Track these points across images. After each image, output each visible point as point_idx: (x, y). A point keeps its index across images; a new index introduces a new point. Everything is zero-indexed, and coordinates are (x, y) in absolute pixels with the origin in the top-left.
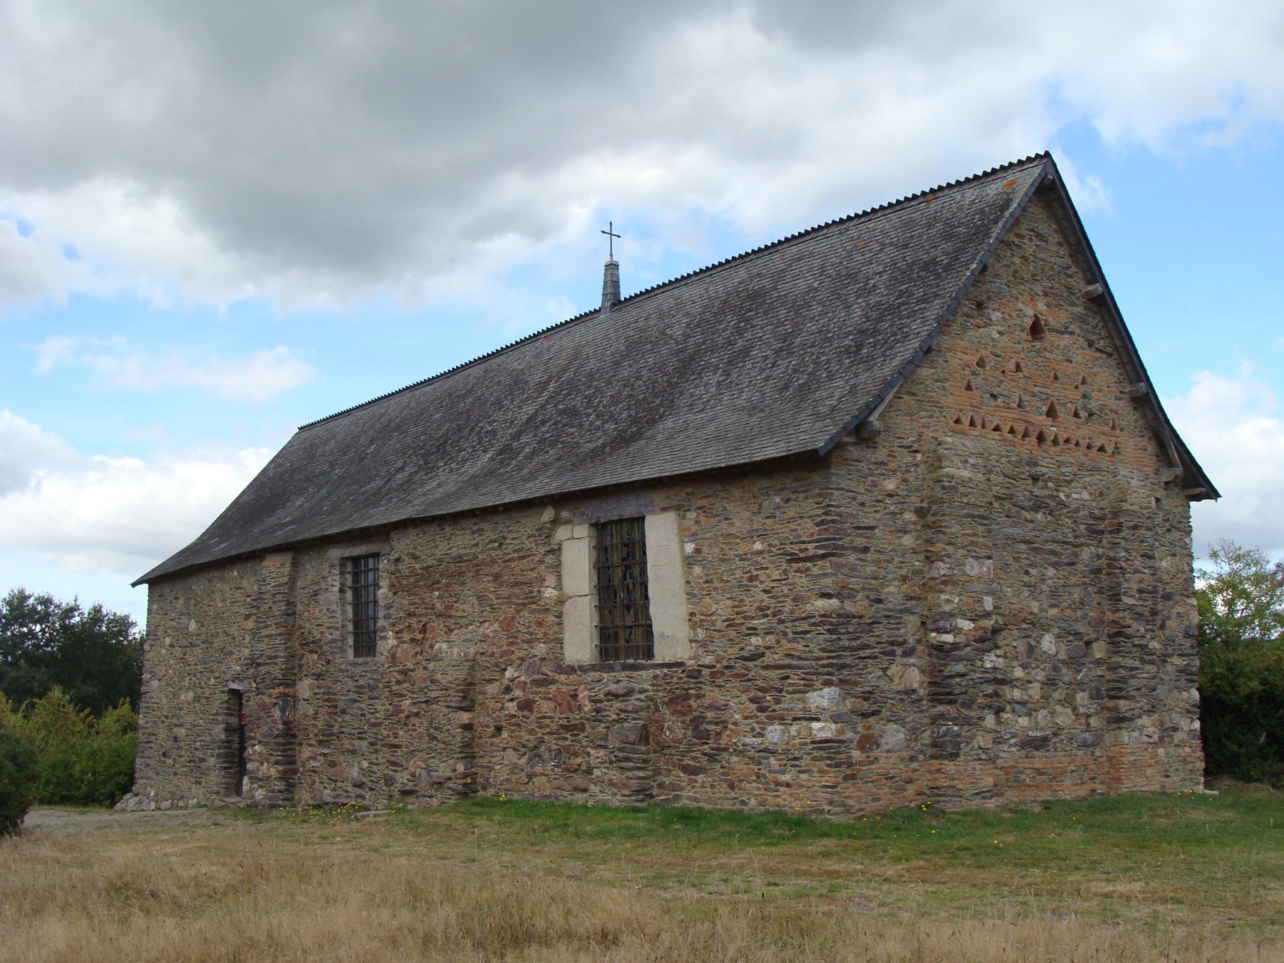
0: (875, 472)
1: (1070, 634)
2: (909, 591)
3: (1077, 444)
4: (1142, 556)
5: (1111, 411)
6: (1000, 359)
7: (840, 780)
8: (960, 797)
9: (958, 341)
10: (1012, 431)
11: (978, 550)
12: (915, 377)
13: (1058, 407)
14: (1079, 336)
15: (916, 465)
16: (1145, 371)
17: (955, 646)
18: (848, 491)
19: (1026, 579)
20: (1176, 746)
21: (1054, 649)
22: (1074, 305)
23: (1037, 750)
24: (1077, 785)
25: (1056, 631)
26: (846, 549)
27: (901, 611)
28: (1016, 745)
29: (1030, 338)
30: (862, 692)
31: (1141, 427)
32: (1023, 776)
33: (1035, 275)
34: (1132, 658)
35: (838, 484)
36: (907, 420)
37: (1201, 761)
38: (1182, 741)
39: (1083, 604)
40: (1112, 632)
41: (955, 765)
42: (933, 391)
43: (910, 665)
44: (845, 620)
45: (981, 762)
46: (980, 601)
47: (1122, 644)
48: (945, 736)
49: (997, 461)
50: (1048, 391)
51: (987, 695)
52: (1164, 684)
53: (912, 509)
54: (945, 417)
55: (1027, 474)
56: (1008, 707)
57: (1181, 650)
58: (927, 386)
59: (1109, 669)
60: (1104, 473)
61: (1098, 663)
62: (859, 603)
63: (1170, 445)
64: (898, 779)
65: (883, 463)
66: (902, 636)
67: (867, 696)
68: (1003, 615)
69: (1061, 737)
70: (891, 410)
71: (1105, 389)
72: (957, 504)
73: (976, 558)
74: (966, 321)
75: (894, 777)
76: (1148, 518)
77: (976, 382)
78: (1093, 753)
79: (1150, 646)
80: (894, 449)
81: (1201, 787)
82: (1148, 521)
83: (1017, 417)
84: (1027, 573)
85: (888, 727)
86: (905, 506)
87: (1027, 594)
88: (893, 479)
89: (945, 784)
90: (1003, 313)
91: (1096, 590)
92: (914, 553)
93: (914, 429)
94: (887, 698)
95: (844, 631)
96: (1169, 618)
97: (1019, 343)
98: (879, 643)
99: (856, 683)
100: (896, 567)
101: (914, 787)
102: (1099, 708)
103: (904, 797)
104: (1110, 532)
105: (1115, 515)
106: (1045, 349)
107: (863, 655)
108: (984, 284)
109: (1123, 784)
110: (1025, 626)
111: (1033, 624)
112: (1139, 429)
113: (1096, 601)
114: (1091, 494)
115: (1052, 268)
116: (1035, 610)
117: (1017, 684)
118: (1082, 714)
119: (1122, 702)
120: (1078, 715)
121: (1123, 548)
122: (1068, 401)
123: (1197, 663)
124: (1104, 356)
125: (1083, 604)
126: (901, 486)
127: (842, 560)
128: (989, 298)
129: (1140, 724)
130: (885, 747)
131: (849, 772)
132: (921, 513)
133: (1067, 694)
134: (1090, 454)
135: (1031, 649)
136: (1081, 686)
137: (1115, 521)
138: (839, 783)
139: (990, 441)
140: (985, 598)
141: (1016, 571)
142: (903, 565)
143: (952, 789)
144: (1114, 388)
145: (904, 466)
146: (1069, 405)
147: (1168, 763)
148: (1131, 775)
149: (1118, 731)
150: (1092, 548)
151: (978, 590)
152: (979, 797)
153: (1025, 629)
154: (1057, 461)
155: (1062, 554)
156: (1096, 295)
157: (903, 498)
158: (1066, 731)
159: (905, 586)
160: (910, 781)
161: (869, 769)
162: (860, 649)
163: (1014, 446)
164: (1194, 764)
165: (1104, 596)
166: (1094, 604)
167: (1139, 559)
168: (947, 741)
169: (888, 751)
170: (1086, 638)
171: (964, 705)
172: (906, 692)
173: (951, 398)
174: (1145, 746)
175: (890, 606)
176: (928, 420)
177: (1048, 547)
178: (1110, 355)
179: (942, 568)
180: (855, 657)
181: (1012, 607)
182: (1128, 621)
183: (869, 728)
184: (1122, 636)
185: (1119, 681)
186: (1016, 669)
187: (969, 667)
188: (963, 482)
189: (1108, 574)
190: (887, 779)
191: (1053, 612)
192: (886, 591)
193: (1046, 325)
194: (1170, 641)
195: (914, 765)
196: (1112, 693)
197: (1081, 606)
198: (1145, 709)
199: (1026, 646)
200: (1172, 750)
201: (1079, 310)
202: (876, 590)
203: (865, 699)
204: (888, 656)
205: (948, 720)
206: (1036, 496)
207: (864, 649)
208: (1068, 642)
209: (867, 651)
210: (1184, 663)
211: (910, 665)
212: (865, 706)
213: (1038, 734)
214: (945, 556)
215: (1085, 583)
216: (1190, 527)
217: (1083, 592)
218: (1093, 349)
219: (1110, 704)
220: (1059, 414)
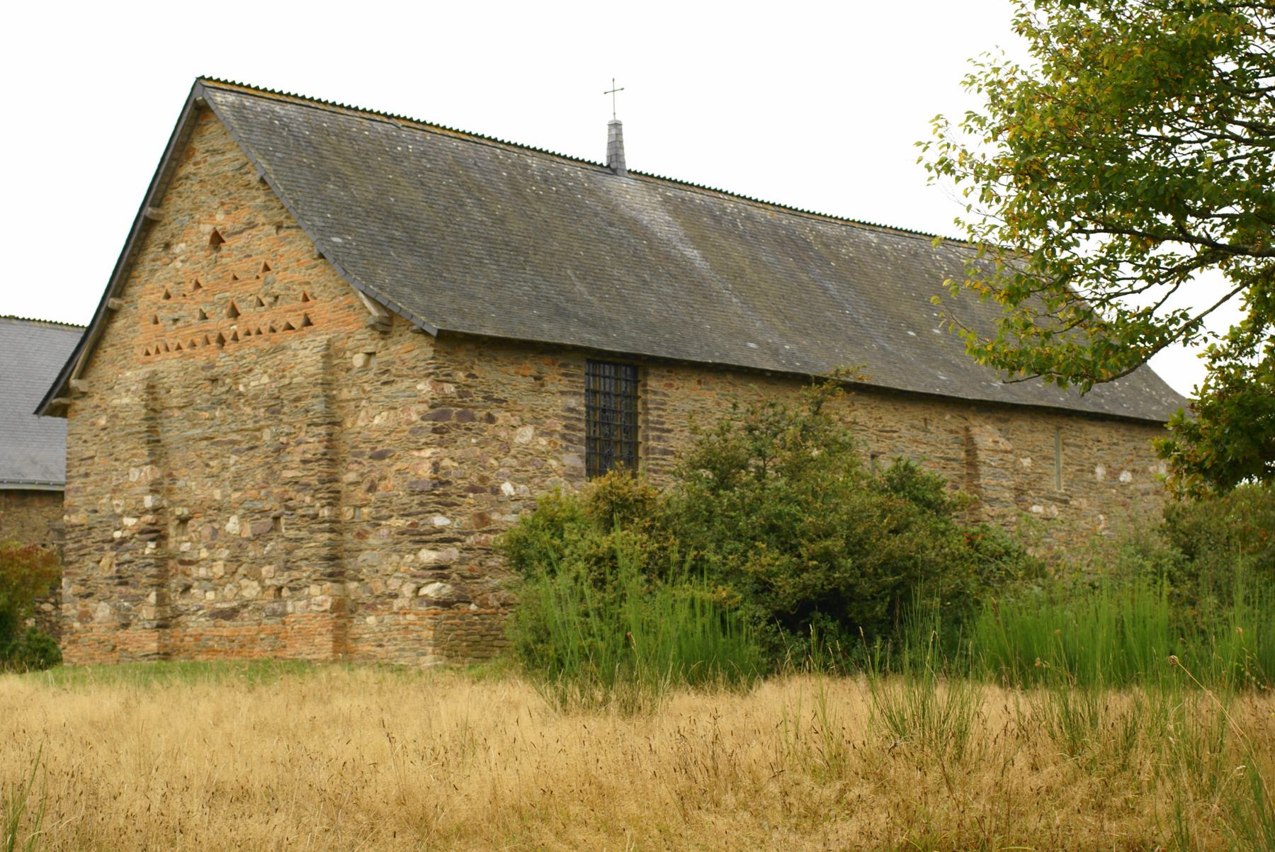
3: (259, 332)
19: (208, 470)
22: (254, 198)
25: (241, 512)
32: (210, 643)
46: (141, 501)
52: (373, 550)
56: (196, 584)
57: (405, 509)
67: (84, 582)
84: (207, 465)
90: (186, 242)
96: (383, 478)
110: (211, 512)
115: (226, 177)
118: (269, 586)
128: (173, 236)
130: (97, 620)
131: (72, 638)
136: (268, 560)
146: (250, 298)
147: (381, 631)
170: (273, 514)
175: (103, 513)
183: (85, 606)
191: (236, 495)
200: (388, 619)
203: (82, 585)
215: (267, 463)
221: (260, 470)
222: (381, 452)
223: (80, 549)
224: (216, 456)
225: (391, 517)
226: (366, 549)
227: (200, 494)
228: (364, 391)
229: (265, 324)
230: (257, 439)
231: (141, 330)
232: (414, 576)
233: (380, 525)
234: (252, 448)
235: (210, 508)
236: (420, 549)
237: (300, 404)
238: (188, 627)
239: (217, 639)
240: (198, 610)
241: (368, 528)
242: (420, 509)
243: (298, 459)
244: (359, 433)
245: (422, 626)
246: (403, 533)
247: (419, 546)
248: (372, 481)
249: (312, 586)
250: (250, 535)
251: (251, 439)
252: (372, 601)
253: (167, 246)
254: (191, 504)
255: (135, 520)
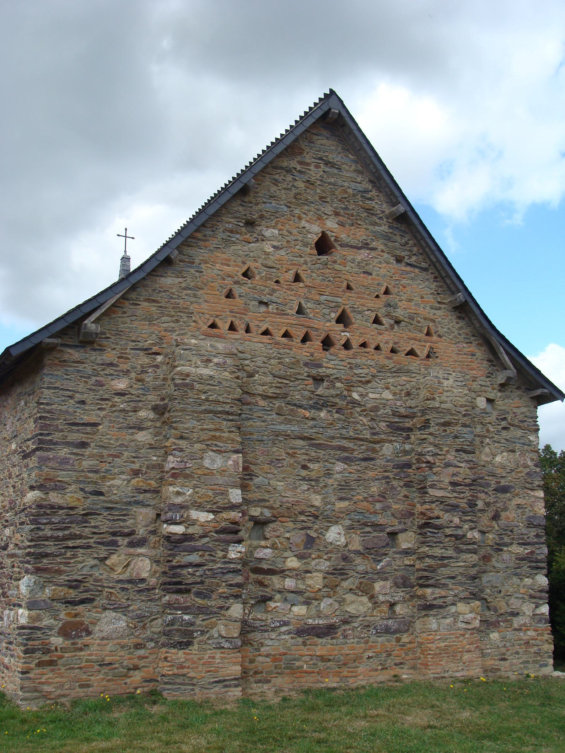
0: (101, 373)
1: (368, 526)
2: (141, 484)
3: (377, 348)
4: (457, 451)
5: (425, 319)
6: (274, 270)
7: (33, 665)
8: (194, 685)
9: (219, 255)
10: (286, 335)
11: (218, 443)
12: (158, 286)
13: (351, 315)
14: (383, 251)
15: (157, 366)
16: (462, 282)
17: (186, 537)
18: (62, 389)
19: (304, 473)
20: (515, 629)
21: (343, 540)
23: (319, 637)
24: (377, 670)
25: (348, 522)
26: (56, 443)
27: (129, 503)
28: (289, 633)
29: (315, 252)
30: (69, 581)
31: (467, 334)
33: (325, 198)
34: (444, 548)
35: (51, 383)
36: (145, 325)
37: (550, 643)
38: (524, 625)
39: (384, 497)
40: (420, 523)
41: (184, 653)
42: (179, 297)
43: (139, 555)
44: (48, 511)
45: (223, 650)
46: (224, 494)
47: (429, 534)
48: (173, 625)
49: (264, 363)
50: (339, 300)
51: (231, 585)
52: (498, 572)
53: (150, 407)
54: (194, 321)
55: (306, 374)
57: (523, 539)
58: (173, 293)
59: (419, 558)
60: (414, 375)
61: (406, 553)
62: (68, 494)
63: (499, 349)
64: (117, 666)
65: (111, 364)
66: (128, 527)
67: (74, 584)
68: (271, 508)
69: (353, 624)
70: (125, 315)
71: (418, 299)
72: (191, 400)
73: (219, 452)
74: (230, 236)
75: (110, 664)
76: (464, 416)
77: (237, 291)
78: (398, 640)
79: (469, 535)
80: (128, 351)
81: (551, 668)
82: (465, 419)
83: (295, 322)
85: (103, 615)
86: (140, 404)
87: (305, 487)
88: (124, 379)
89: (170, 673)
91: (402, 483)
92: (151, 448)
93: (153, 333)
94: (104, 587)
95: (45, 521)
96: (505, 509)
97: (301, 256)
98: (94, 533)
99: (60, 572)
100: (126, 462)
101: (142, 674)
102: (408, 596)
103: (126, 683)
104: (420, 429)
105: (424, 412)
106: (335, 262)
107: (71, 545)
108: (257, 204)
109: (429, 669)
110: (303, 518)
111: (316, 517)
112: (463, 336)
113: (402, 494)
114: (394, 394)
115: (345, 192)
116: (317, 503)
117: (290, 574)
118: (383, 602)
119: (429, 591)
120: (376, 603)
121: (431, 443)
122: (365, 309)
123: (546, 550)
124: (417, 270)
125: (384, 497)
126: (135, 386)
127: (51, 454)
128: (262, 217)
129: (453, 611)
132: (159, 410)
133: (361, 583)
134: (395, 358)
135: (310, 541)
136: (382, 575)
137: (423, 418)
138: (32, 669)
139: (256, 345)
140: (230, 490)
141: (291, 465)
142: (136, 460)
143: (182, 678)
144: (431, 298)
145: (139, 366)
148: (440, 661)
149: (426, 618)
150: (395, 444)
151: (220, 483)
152: (221, 685)
153: (303, 521)
154: (349, 363)
155: (353, 450)
156: (398, 214)
157: (139, 397)
158: (360, 619)
159: (137, 479)
160: (136, 668)
161: (76, 655)
162: (68, 539)
163: (290, 349)
164: (540, 647)
165: (414, 489)
166: (400, 497)
167: (454, 453)
168: (174, 630)
169: (103, 639)
170: (388, 530)
171: (199, 594)
172: (130, 581)
173: (205, 306)
174: (462, 632)
176: (173, 325)
177: (335, 443)
178: (425, 270)
179: (172, 462)
180: (61, 546)
181: (285, 500)
182: (437, 513)
184: (429, 527)
185: (426, 570)
186: (289, 560)
187: (207, 557)
188: (201, 380)
189: (418, 469)
190: (100, 665)
192: (108, 484)
193: (336, 240)
194: (509, 530)
195: (142, 652)
196: (421, 582)
197: (381, 499)
198: (462, 595)
199: (304, 538)
200: (509, 634)
201: (384, 228)
202: (96, 483)
204: (106, 546)
205: (176, 609)
206: (317, 395)
207: (74, 539)
208: (363, 533)
209: (79, 541)
210: (526, 551)
211: (139, 555)
212: (72, 594)
213: (321, 622)
214: (174, 450)
215: (387, 477)
216: (538, 425)
217: (385, 486)
218: (403, 264)
219: (420, 592)
220: (353, 320)
221: (377, 483)
222: (504, 486)
223: (65, 538)
224: (316, 460)
225: (512, 544)
226: (491, 571)
227: (290, 497)
228: (488, 431)
229: (387, 343)
230: (374, 451)
231: (206, 297)
232: (534, 597)
233: (502, 550)
234: (365, 459)
235: (302, 513)
236: (536, 574)
237: (449, 429)
238: (262, 645)
239: (308, 658)
240: (281, 626)
241: (492, 552)
242: (536, 540)
243: (447, 481)
244: (484, 466)
245: (541, 641)
246: (523, 559)
247: (535, 572)
248: (497, 511)
249: (459, 604)
250: (360, 548)
251: (368, 450)
252: (494, 619)
253: (250, 224)
254: (277, 505)
255: (211, 516)
